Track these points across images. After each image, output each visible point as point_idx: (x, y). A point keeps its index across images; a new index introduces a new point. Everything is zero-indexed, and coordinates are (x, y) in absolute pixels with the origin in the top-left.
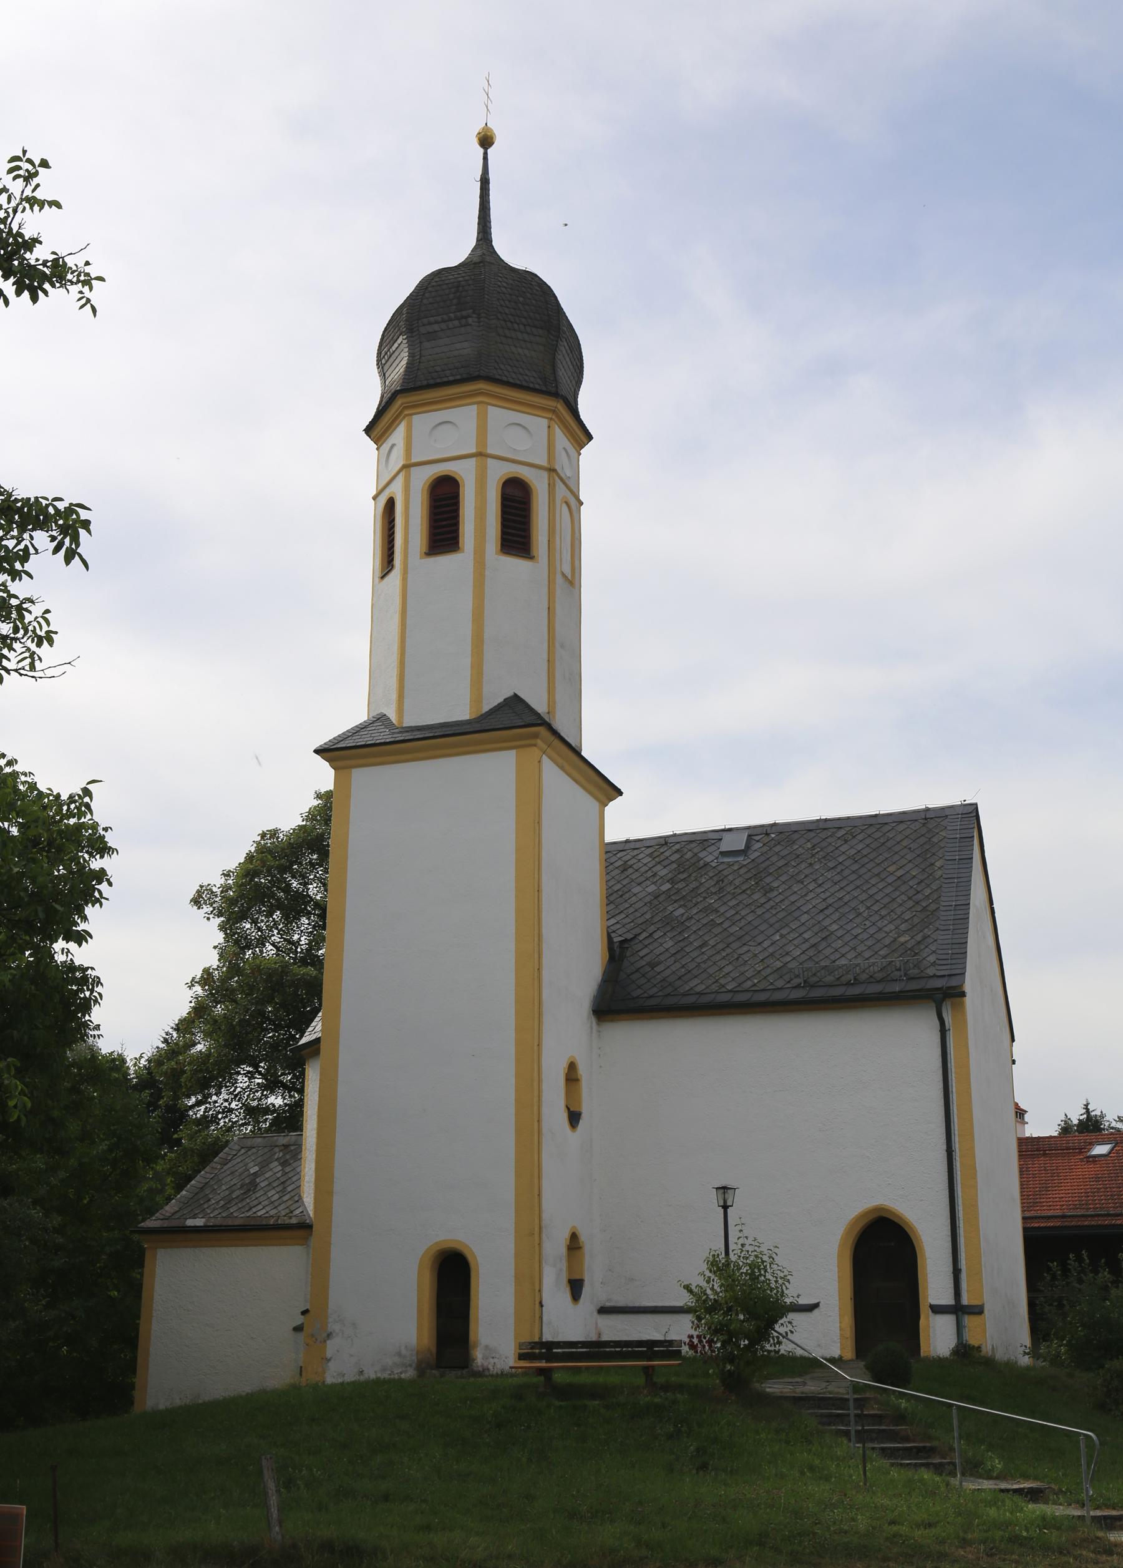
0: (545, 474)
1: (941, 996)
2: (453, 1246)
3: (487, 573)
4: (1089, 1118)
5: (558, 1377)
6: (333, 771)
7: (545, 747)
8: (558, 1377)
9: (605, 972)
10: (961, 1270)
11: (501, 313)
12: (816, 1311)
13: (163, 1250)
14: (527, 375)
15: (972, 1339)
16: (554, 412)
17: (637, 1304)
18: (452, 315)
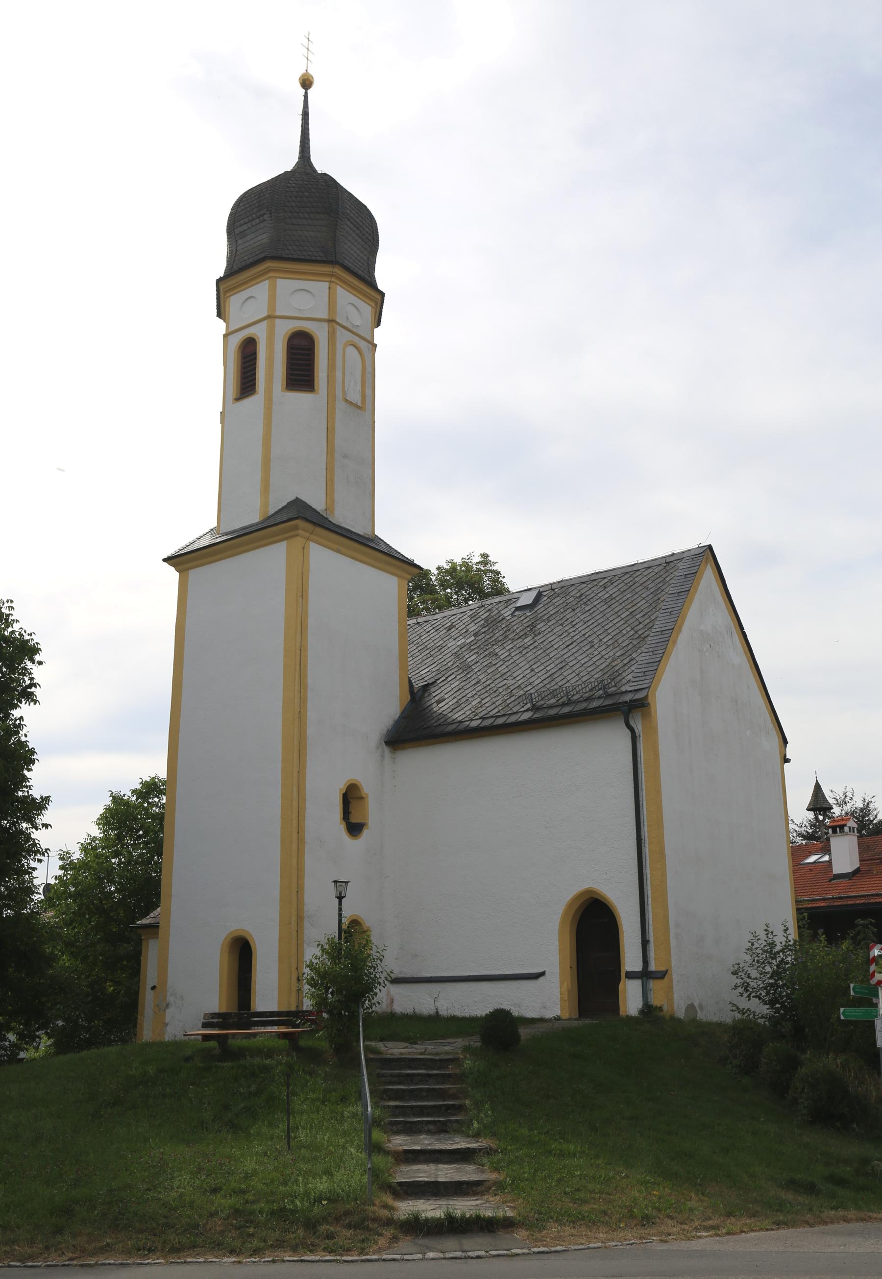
0: (326, 325)
1: (626, 707)
2: (241, 934)
3: (274, 407)
4: (114, 798)
5: (231, 1041)
6: (178, 574)
7: (307, 535)
8: (234, 1043)
9: (404, 711)
10: (649, 941)
11: (288, 207)
12: (542, 979)
13: (152, 940)
14: (311, 251)
15: (655, 1001)
16: (332, 275)
17: (419, 975)
18: (254, 216)
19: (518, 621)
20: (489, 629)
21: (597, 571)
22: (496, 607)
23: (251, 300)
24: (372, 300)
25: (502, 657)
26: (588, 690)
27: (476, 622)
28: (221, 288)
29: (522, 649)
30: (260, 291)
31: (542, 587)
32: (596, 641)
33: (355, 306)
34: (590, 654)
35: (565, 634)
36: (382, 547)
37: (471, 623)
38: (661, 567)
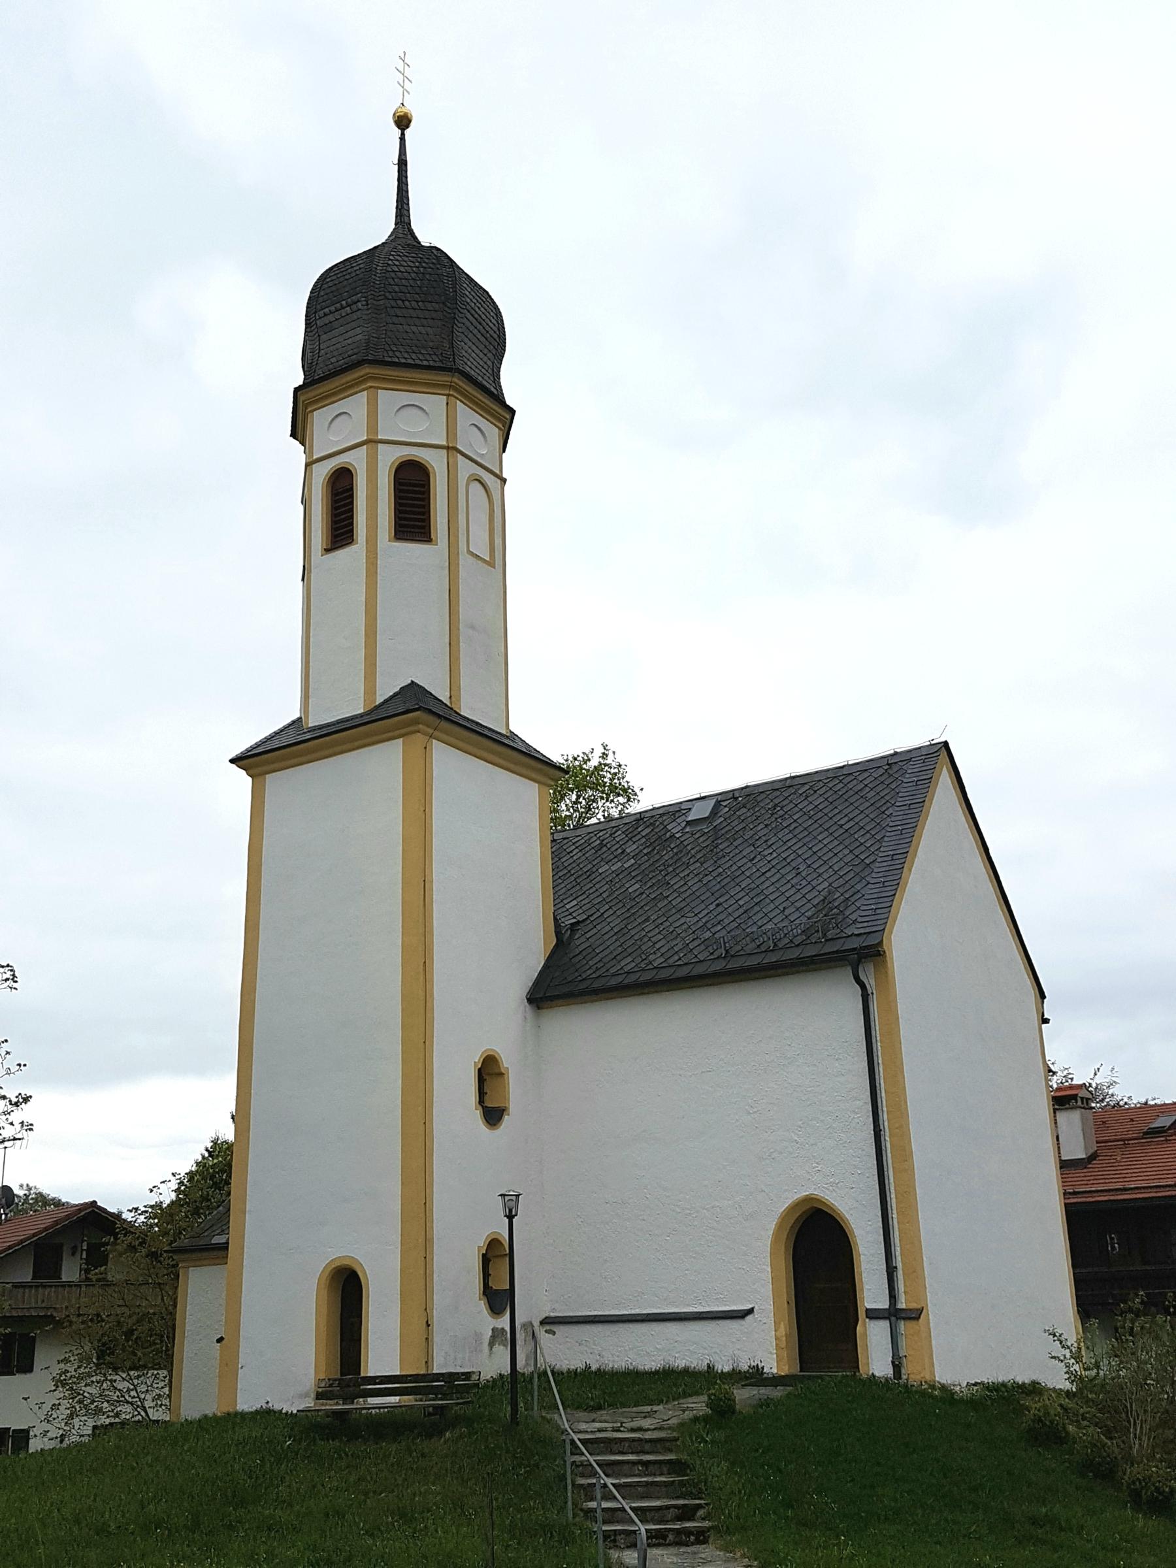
6: (250, 779)
7: (431, 731)
10: (896, 1267)
12: (749, 1318)
19: (692, 840)
20: (653, 850)
21: (792, 775)
22: (660, 820)
23: (343, 417)
24: (499, 420)
25: (675, 887)
26: (799, 931)
27: (634, 839)
28: (301, 398)
29: (701, 876)
30: (356, 405)
31: (720, 794)
32: (802, 867)
33: (479, 429)
34: (797, 884)
35: (759, 857)
36: (519, 746)
37: (628, 841)
38: (881, 771)
